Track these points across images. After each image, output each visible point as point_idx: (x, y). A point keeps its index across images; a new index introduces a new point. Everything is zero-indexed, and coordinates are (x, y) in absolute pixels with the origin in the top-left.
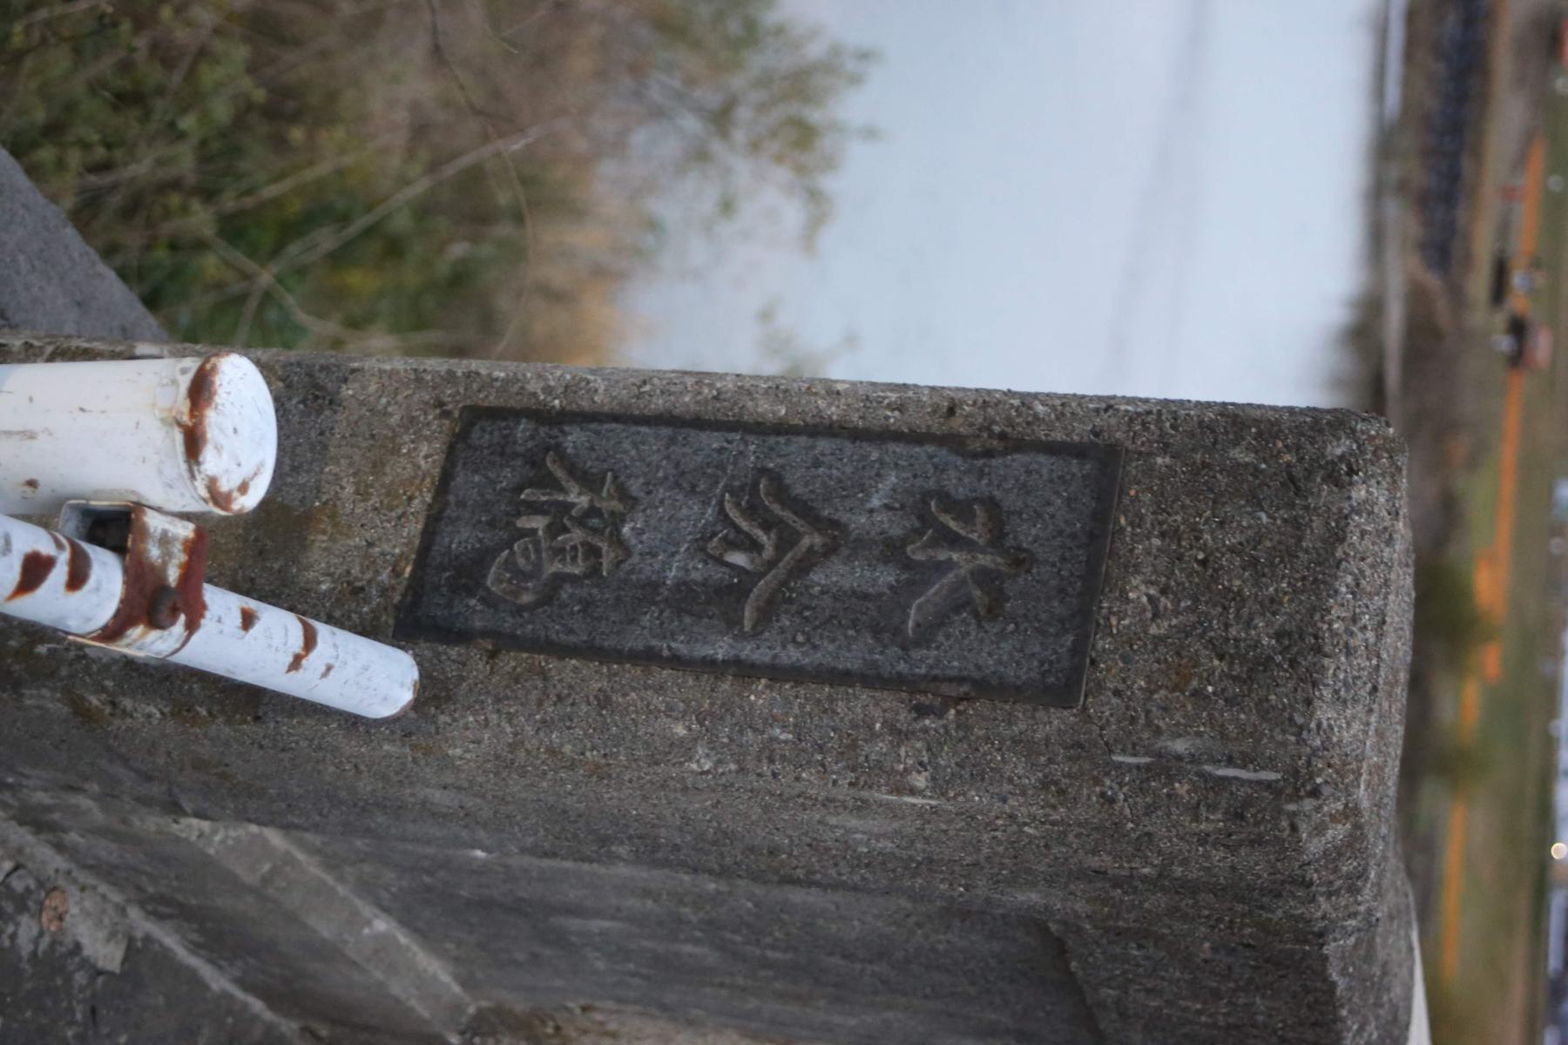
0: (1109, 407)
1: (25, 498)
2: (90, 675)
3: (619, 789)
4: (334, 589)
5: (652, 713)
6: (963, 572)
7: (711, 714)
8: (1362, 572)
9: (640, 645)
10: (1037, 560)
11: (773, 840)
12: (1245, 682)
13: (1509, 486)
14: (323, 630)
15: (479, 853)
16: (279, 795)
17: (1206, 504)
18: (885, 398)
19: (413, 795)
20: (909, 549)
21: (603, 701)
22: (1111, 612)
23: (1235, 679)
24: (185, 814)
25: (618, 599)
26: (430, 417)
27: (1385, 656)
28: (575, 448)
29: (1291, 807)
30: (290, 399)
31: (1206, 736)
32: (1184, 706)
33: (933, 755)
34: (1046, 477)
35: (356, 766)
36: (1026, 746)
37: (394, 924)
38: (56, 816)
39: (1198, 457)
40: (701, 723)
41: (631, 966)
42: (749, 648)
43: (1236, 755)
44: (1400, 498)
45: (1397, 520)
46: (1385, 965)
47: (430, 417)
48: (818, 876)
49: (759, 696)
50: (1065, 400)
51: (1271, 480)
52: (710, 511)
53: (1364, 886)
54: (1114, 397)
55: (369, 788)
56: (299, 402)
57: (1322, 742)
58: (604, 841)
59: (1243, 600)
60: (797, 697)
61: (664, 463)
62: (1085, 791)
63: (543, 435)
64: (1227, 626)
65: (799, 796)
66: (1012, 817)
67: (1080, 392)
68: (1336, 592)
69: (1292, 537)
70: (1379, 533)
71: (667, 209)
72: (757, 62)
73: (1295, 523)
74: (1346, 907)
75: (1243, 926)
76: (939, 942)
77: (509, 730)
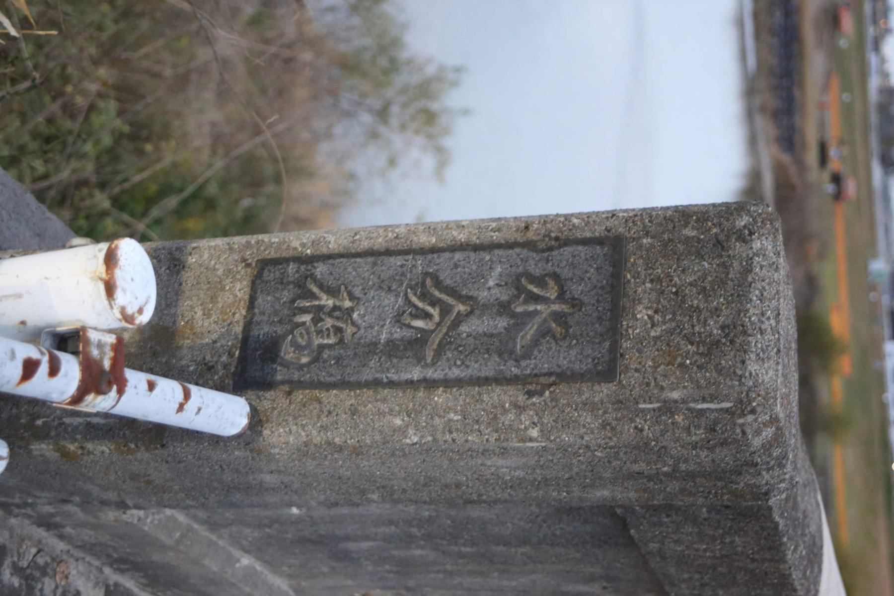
0: (613, 215)
1: (20, 332)
2: (67, 433)
3: (368, 461)
4: (198, 368)
5: (381, 414)
6: (544, 315)
7: (414, 410)
8: (764, 288)
9: (370, 378)
10: (584, 304)
11: (457, 479)
12: (707, 355)
13: (843, 267)
14: (194, 389)
15: (295, 510)
16: (180, 489)
17: (674, 261)
18: (489, 226)
19: (254, 479)
20: (513, 306)
21: (354, 412)
22: (628, 327)
23: (701, 354)
24: (128, 508)
25: (355, 354)
26: (240, 268)
27: (782, 332)
28: (322, 274)
29: (741, 421)
30: (161, 268)
31: (689, 388)
32: (675, 373)
33: (540, 418)
34: (583, 257)
35: (221, 466)
36: (591, 406)
37: (253, 560)
38: (58, 519)
39: (666, 236)
40: (409, 416)
41: (387, 567)
42: (431, 372)
43: (706, 396)
44: (780, 245)
45: (779, 257)
46: (804, 512)
47: (240, 268)
48: (484, 497)
49: (440, 397)
50: (589, 215)
51: (707, 243)
52: (400, 300)
53: (787, 463)
54: (616, 210)
55: (230, 479)
56: (165, 270)
57: (754, 383)
58: (363, 492)
59: (700, 311)
60: (460, 395)
61: (372, 276)
62: (626, 427)
63: (303, 270)
64: (693, 326)
65: (468, 451)
66: (587, 447)
67: (596, 210)
68: (751, 300)
69: (723, 273)
70: (770, 266)
71: (358, 166)
72: (401, 79)
73: (724, 265)
74: (778, 476)
75: (723, 494)
76: (556, 529)
77: (303, 434)
